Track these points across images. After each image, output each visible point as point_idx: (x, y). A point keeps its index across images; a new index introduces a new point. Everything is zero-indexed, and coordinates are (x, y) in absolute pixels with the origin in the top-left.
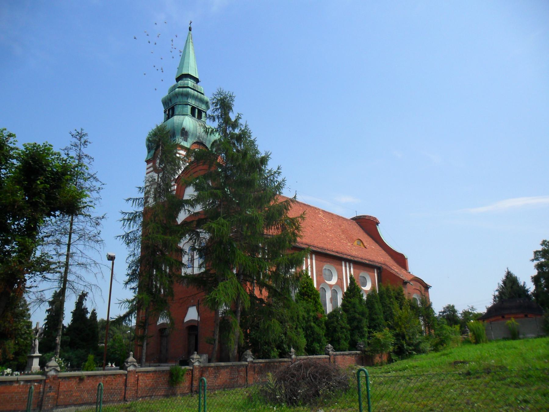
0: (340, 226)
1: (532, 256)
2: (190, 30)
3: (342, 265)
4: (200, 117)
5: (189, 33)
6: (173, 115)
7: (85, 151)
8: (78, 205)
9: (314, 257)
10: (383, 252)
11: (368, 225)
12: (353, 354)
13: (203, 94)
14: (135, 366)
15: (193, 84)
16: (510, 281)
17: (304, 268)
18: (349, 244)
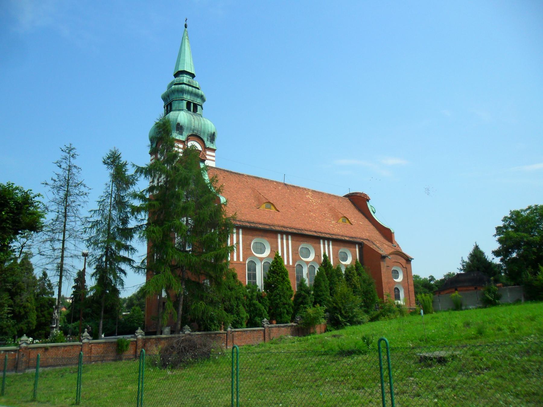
0: (328, 205)
1: (495, 232)
2: (186, 27)
3: (320, 243)
4: (195, 110)
5: (185, 30)
6: (171, 110)
7: (73, 162)
8: (36, 225)
9: (290, 237)
10: (372, 227)
11: (359, 201)
12: (289, 326)
13: (198, 89)
14: (88, 339)
15: (188, 79)
16: (477, 256)
17: (229, 259)
18: (333, 222)
